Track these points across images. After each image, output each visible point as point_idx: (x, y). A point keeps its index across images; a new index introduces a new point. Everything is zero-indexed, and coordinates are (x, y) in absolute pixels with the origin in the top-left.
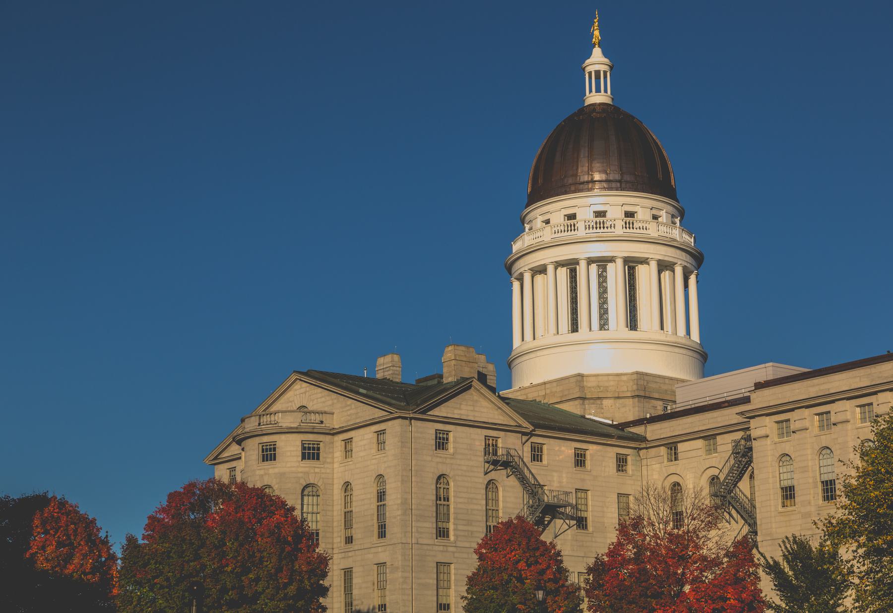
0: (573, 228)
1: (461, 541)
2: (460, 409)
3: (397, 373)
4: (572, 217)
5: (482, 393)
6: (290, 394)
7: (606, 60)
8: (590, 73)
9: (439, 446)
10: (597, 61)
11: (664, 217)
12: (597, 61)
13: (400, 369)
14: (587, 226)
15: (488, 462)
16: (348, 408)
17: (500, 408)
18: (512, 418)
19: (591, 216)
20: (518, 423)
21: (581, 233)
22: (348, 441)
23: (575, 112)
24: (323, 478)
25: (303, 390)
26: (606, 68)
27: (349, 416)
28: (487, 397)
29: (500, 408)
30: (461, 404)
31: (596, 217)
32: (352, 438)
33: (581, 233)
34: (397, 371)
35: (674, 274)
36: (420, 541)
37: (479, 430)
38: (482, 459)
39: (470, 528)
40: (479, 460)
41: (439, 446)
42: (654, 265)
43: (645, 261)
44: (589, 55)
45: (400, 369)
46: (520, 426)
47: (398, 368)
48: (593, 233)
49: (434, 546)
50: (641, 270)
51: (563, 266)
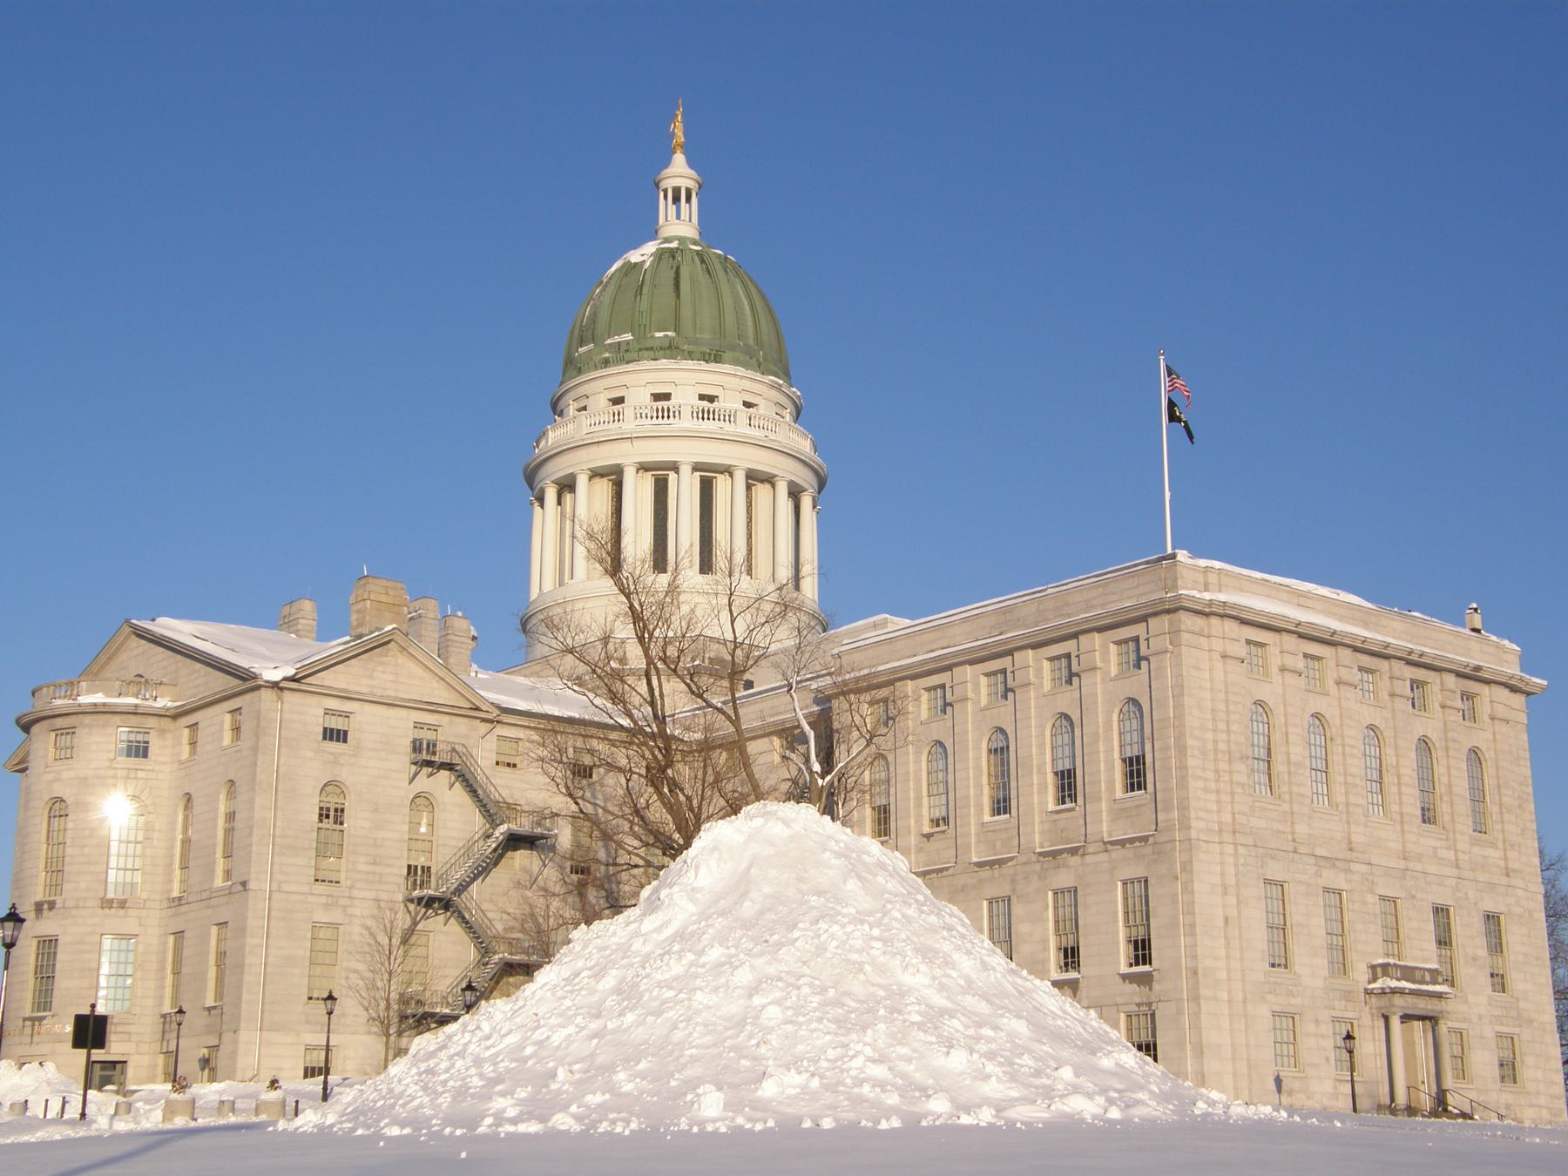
0: (618, 417)
1: (360, 889)
2: (371, 677)
3: (310, 628)
4: (619, 401)
5: (411, 654)
6: (123, 657)
7: (692, 173)
8: (666, 191)
9: (885, 809)
10: (679, 173)
11: (764, 408)
12: (679, 173)
13: (315, 623)
14: (638, 415)
15: (415, 764)
16: (196, 675)
17: (442, 679)
18: (468, 699)
19: (646, 399)
20: (474, 704)
21: (629, 425)
22: (193, 727)
23: (1130, 983)
24: (151, 788)
25: (141, 649)
26: (691, 184)
27: (196, 687)
28: (419, 661)
29: (442, 679)
30: (374, 670)
31: (655, 400)
32: (197, 723)
33: (629, 425)
34: (308, 625)
35: (774, 488)
36: (286, 887)
37: (404, 712)
38: (408, 759)
39: (378, 869)
40: (402, 760)
41: (885, 809)
42: (740, 477)
43: (728, 471)
44: (667, 162)
45: (315, 623)
46: (477, 709)
47: (311, 622)
48: (647, 426)
49: (310, 896)
50: (721, 484)
51: (602, 476)
